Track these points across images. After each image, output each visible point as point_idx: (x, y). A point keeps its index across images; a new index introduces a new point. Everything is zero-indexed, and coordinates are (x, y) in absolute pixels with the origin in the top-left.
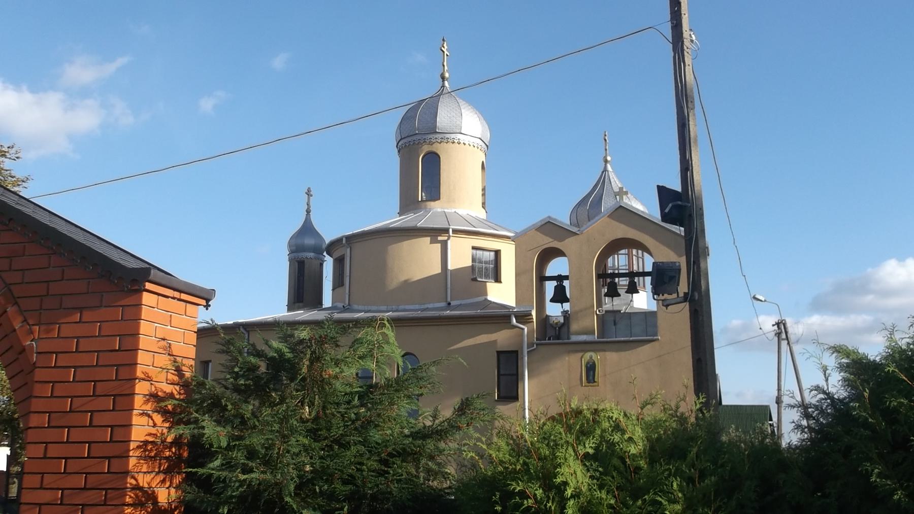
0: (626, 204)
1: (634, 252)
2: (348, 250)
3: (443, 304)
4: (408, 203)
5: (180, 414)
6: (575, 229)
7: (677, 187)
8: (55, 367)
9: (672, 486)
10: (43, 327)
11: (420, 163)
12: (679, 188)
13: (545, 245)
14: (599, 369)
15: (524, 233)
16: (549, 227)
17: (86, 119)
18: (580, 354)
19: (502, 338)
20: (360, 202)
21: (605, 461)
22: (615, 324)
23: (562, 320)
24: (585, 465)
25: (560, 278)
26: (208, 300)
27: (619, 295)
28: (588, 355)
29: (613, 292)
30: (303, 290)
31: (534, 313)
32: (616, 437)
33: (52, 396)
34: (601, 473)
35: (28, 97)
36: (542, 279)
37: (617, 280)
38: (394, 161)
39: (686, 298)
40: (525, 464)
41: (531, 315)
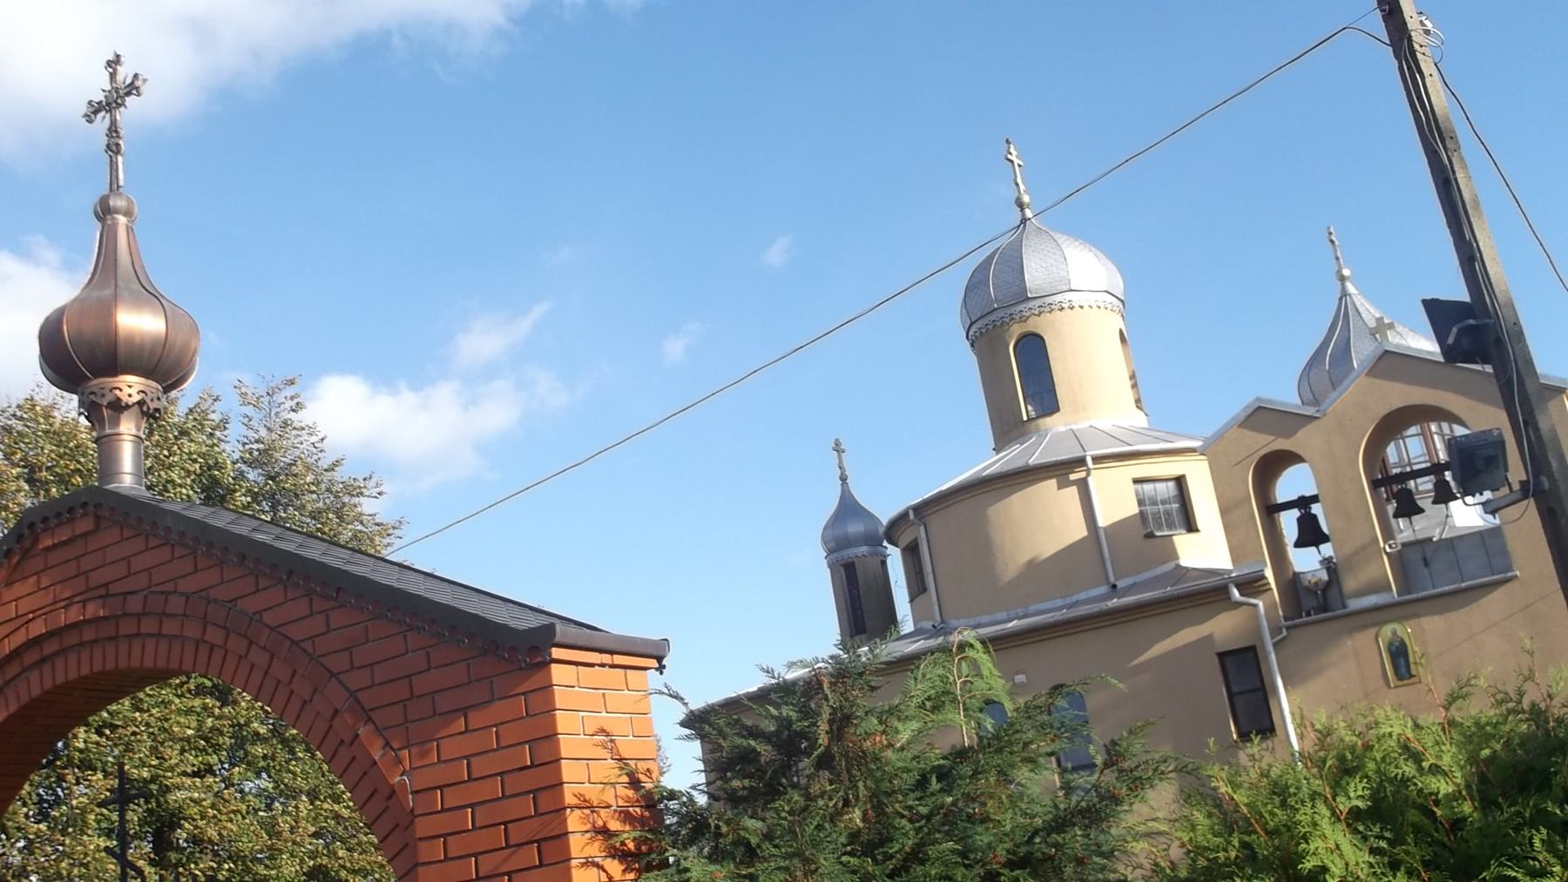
0: (1397, 346)
1: (1434, 427)
2: (922, 529)
3: (1104, 589)
4: (1007, 428)
5: (649, 854)
6: (1310, 411)
7: (1461, 294)
8: (443, 810)
9: (1532, 845)
10: (414, 750)
11: (1015, 362)
12: (1466, 298)
13: (1264, 451)
14: (1414, 649)
15: (1219, 436)
16: (1261, 416)
17: (499, 413)
18: (1373, 631)
19: (1222, 628)
20: (930, 443)
21: (1389, 814)
22: (1426, 563)
23: (1324, 576)
24: (1356, 831)
25: (1303, 503)
26: (660, 659)
27: (1421, 511)
28: (1387, 631)
29: (1409, 508)
30: (863, 609)
31: (1269, 573)
32: (1409, 769)
33: (447, 859)
34: (1391, 842)
35: (408, 398)
36: (1271, 510)
37: (1412, 484)
38: (966, 364)
39: (1526, 491)
40: (1245, 845)
41: (1264, 577)
